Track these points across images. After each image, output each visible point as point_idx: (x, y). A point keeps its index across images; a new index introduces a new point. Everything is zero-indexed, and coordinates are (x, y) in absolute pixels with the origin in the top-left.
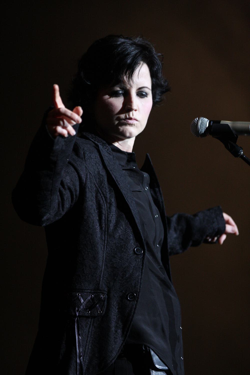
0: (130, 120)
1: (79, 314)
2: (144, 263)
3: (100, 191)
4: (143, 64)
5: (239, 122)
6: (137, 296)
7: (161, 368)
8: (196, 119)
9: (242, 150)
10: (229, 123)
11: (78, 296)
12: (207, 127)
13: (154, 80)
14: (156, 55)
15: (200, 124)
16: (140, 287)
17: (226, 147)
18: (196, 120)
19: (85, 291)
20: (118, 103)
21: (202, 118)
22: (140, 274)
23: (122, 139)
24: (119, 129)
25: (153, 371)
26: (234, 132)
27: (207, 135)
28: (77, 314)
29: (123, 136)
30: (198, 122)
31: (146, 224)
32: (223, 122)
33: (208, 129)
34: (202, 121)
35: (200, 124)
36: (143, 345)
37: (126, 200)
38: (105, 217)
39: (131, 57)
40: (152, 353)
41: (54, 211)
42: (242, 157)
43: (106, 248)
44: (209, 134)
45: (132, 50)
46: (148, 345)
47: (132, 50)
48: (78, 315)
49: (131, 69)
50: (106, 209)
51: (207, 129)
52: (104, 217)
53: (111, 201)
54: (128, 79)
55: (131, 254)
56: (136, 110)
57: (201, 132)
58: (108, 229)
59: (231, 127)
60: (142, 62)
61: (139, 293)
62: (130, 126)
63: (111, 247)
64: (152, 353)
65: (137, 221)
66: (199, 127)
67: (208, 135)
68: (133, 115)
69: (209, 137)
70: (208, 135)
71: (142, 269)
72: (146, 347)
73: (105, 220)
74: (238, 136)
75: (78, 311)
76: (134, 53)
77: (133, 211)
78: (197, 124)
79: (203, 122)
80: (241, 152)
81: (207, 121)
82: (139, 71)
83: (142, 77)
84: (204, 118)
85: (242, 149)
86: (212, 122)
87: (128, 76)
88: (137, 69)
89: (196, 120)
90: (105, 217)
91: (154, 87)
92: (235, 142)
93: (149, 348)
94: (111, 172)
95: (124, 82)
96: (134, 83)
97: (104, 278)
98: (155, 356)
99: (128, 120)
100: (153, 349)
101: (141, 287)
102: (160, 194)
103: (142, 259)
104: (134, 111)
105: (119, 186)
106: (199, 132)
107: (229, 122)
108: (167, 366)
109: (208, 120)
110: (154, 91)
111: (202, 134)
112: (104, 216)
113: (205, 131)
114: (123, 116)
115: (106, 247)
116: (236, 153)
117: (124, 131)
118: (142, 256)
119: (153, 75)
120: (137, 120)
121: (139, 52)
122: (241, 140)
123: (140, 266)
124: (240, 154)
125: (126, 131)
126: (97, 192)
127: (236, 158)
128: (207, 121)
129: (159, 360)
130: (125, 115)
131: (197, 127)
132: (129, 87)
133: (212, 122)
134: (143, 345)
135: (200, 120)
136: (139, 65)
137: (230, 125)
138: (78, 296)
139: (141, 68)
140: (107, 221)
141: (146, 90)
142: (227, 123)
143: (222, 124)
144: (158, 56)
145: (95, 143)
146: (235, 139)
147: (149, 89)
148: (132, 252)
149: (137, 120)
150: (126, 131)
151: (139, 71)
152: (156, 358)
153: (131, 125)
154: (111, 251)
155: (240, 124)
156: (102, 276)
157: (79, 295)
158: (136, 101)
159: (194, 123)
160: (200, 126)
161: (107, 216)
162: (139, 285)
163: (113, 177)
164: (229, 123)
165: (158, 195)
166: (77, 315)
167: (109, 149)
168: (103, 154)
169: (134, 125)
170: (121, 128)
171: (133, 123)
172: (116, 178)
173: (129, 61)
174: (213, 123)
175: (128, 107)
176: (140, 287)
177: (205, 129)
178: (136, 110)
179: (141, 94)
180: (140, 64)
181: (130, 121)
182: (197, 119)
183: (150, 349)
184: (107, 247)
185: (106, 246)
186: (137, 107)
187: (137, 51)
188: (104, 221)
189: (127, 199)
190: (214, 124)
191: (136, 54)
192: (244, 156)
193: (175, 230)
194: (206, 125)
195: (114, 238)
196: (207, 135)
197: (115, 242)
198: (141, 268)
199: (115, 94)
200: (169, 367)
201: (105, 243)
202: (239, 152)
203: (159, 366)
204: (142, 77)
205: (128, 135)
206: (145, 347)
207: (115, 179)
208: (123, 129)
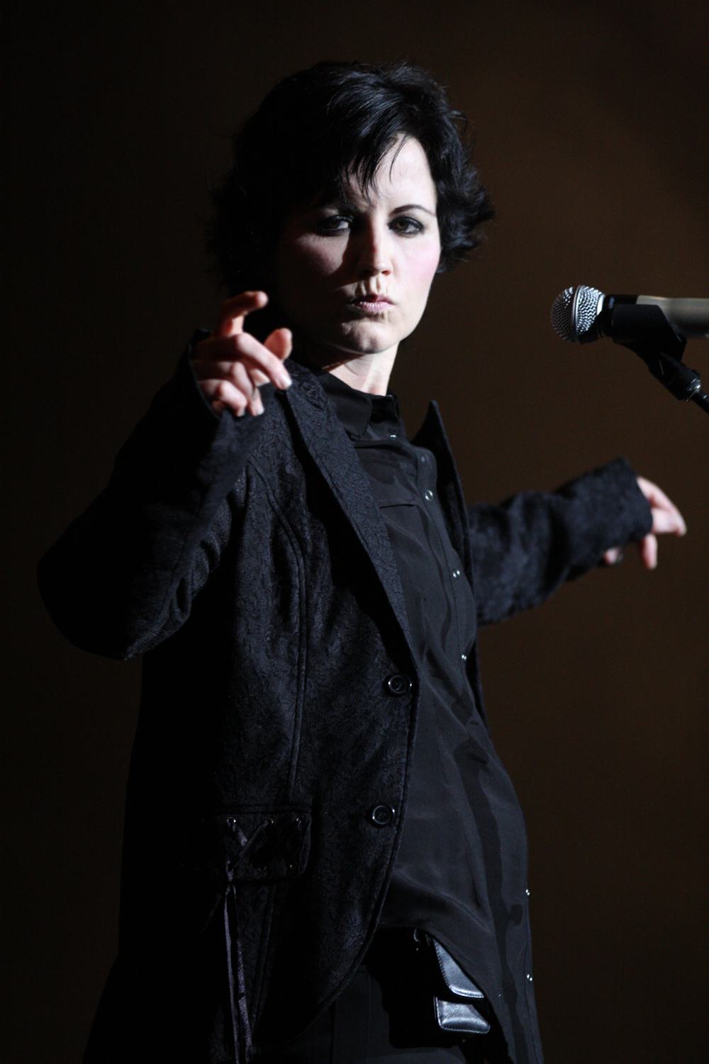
0: (371, 304)
1: (235, 875)
2: (399, 847)
3: (287, 524)
4: (404, 140)
5: (690, 300)
6: (399, 814)
7: (463, 995)
8: (568, 292)
9: (699, 378)
10: (660, 301)
11: (229, 824)
12: (598, 313)
13: (442, 183)
14: (449, 115)
15: (577, 306)
16: (405, 787)
17: (654, 371)
18: (566, 293)
19: (253, 815)
20: (334, 249)
21: (582, 289)
22: (405, 751)
23: (353, 354)
24: (342, 329)
25: (445, 1003)
26: (675, 327)
28: (229, 875)
29: (353, 349)
30: (572, 299)
31: (425, 600)
32: (643, 300)
33: (601, 320)
34: (584, 296)
35: (579, 305)
36: (415, 931)
37: (362, 541)
38: (300, 597)
39: (373, 119)
40: (440, 951)
41: (163, 620)
42: (697, 398)
43: (303, 684)
44: (603, 334)
45: (379, 101)
46: (434, 932)
47: (379, 101)
48: (233, 880)
49: (369, 156)
50: (303, 571)
52: (296, 598)
53: (317, 548)
54: (360, 183)
55: (376, 697)
56: (386, 273)
57: (581, 327)
58: (309, 631)
59: (665, 315)
60: (401, 136)
61: (403, 804)
62: (371, 321)
63: (320, 681)
64: (441, 951)
65: (396, 597)
66: (577, 312)
67: (602, 337)
68: (378, 287)
69: (606, 341)
70: (602, 337)
71: (411, 736)
72: (422, 934)
73: (300, 603)
74: (688, 340)
75: (230, 867)
76: (382, 107)
77: (380, 571)
78: (571, 305)
79: (587, 299)
80: (695, 384)
81: (599, 296)
82: (393, 162)
83: (405, 174)
84: (590, 287)
85: (699, 376)
86: (612, 300)
87: (360, 174)
88: (387, 155)
89: (566, 293)
90: (300, 594)
91: (443, 209)
93: (432, 937)
94: (318, 461)
95: (350, 194)
96: (380, 194)
97: (303, 770)
98: (448, 959)
99: (365, 303)
100: (445, 943)
101: (409, 786)
102: (463, 519)
103: (410, 707)
104: (381, 276)
105: (341, 502)
106: (575, 327)
107: (662, 301)
108: (480, 990)
109: (600, 293)
110: (445, 218)
111: (585, 333)
112: (297, 591)
113: (592, 326)
114: (350, 289)
115: (306, 681)
116: (680, 388)
117: (356, 334)
118: (409, 701)
119: (439, 171)
120: (390, 302)
121: (394, 106)
122: (694, 351)
123: (404, 728)
124: (693, 390)
125: (359, 335)
126: (277, 524)
127: (681, 401)
128: (599, 296)
129: (463, 975)
130: (356, 284)
131: (571, 312)
132: (366, 207)
133: (612, 300)
134: (415, 931)
135: (579, 294)
136: (391, 143)
137: (663, 308)
138: (229, 824)
139: (399, 150)
140: (307, 607)
141: (419, 215)
142: (654, 303)
143: (639, 305)
144: (452, 120)
145: (284, 552)
146: (678, 349)
147: (429, 212)
148: (378, 691)
149: (390, 302)
150: (361, 335)
151: (393, 162)
152: (450, 967)
153: (375, 317)
154: (319, 691)
155: (694, 307)
156: (295, 763)
157: (231, 821)
158: (386, 245)
159: (562, 302)
160: (579, 311)
161: (307, 591)
162: (402, 783)
163: (324, 474)
164: (660, 301)
165: (455, 521)
166: (231, 878)
167: (318, 389)
168: (296, 410)
169: (383, 316)
170: (348, 327)
171: (380, 312)
172: (331, 479)
173: (365, 131)
174: (614, 303)
175: (361, 260)
176: (405, 787)
177: (593, 319)
178: (386, 273)
179: (402, 222)
180: (396, 140)
181: (371, 307)
182: (571, 290)
183: (434, 941)
185: (303, 679)
186: (390, 263)
187: (389, 104)
188: (297, 607)
189: (363, 538)
190: (619, 303)
191: (387, 112)
192: (705, 397)
193: (525, 546)
194: (596, 308)
195: (328, 655)
196: (599, 336)
197: (328, 666)
198: (407, 732)
199: (328, 229)
200: (486, 992)
201: (299, 670)
202: (688, 384)
203: (460, 987)
204: (405, 174)
205: (365, 344)
206: (422, 934)
207: (328, 480)
208: (352, 329)
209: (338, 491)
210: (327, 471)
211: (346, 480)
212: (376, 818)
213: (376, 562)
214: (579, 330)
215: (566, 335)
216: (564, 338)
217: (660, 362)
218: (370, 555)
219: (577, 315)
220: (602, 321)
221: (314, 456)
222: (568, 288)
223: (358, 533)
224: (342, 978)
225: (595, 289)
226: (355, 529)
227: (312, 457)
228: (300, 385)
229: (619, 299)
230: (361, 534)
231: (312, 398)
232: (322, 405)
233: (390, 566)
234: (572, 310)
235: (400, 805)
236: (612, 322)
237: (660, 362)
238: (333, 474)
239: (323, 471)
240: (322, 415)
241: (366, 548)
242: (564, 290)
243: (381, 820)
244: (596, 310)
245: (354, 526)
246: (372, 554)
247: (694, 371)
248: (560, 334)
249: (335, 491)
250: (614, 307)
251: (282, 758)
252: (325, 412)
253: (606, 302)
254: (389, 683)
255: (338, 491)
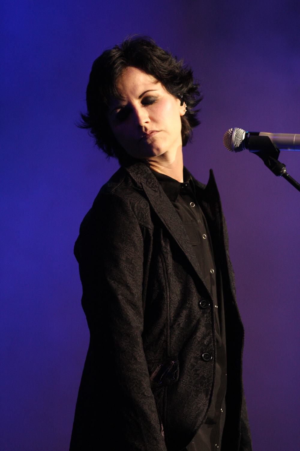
8: (231, 130)
12: (243, 139)
17: (266, 164)
18: (230, 131)
21: (236, 129)
26: (275, 146)
27: (243, 150)
30: (232, 133)
32: (262, 134)
35: (235, 136)
42: (285, 176)
44: (245, 148)
51: (243, 142)
57: (235, 145)
66: (234, 139)
67: (244, 149)
69: (246, 151)
70: (244, 149)
74: (281, 152)
77: (189, 258)
81: (244, 132)
84: (240, 128)
89: (230, 131)
92: (277, 158)
94: (159, 215)
105: (170, 231)
106: (233, 145)
109: (244, 131)
111: (237, 148)
113: (241, 145)
124: (283, 172)
128: (244, 132)
133: (249, 134)
135: (235, 131)
137: (270, 137)
140: (167, 275)
142: (266, 135)
146: (276, 154)
159: (228, 135)
164: (269, 135)
167: (155, 181)
168: (148, 194)
172: (165, 222)
177: (241, 142)
182: (232, 129)
184: (171, 305)
194: (242, 137)
196: (243, 149)
209: (168, 226)
210: (163, 218)
211: (171, 221)
212: (204, 356)
213: (187, 254)
214: (235, 147)
215: (230, 149)
216: (229, 150)
217: (269, 160)
218: (184, 252)
219: (234, 140)
220: (245, 143)
221: (157, 213)
222: (230, 128)
223: (178, 243)
224: (202, 420)
225: (242, 129)
226: (177, 242)
227: (156, 214)
228: (147, 181)
229: (252, 134)
230: (180, 244)
231: (152, 187)
232: (157, 189)
233: (193, 255)
234: (232, 138)
235: (213, 352)
236: (249, 143)
237: (269, 160)
238: (165, 220)
239: (161, 219)
240: (158, 194)
241: (183, 250)
242: (229, 129)
243: (207, 359)
244: (242, 138)
245: (176, 241)
246: (185, 251)
247: (283, 164)
248: (227, 148)
249: (167, 227)
250: (250, 137)
251: (174, 340)
252: (158, 193)
253: (246, 134)
254: (200, 303)
255: (168, 226)
